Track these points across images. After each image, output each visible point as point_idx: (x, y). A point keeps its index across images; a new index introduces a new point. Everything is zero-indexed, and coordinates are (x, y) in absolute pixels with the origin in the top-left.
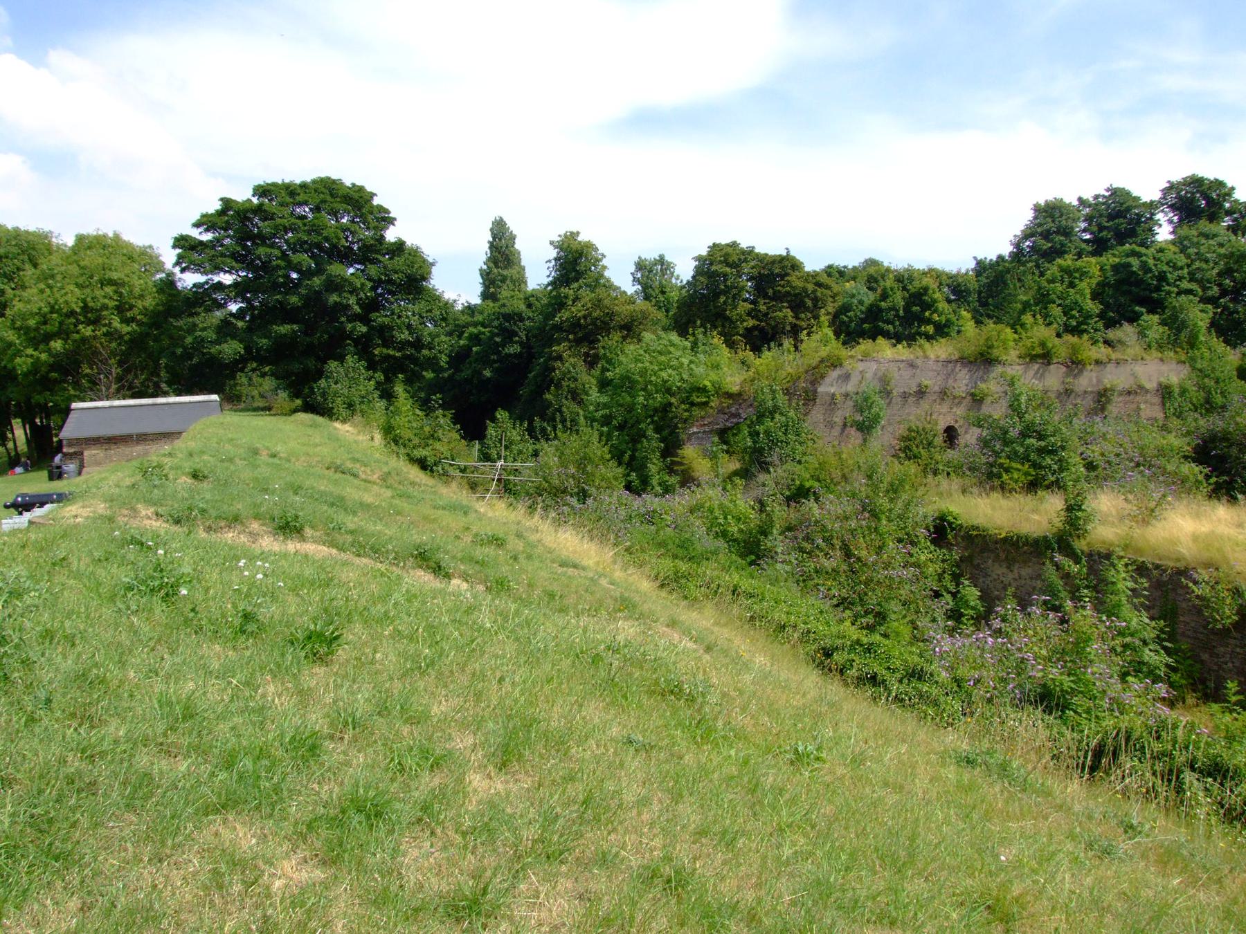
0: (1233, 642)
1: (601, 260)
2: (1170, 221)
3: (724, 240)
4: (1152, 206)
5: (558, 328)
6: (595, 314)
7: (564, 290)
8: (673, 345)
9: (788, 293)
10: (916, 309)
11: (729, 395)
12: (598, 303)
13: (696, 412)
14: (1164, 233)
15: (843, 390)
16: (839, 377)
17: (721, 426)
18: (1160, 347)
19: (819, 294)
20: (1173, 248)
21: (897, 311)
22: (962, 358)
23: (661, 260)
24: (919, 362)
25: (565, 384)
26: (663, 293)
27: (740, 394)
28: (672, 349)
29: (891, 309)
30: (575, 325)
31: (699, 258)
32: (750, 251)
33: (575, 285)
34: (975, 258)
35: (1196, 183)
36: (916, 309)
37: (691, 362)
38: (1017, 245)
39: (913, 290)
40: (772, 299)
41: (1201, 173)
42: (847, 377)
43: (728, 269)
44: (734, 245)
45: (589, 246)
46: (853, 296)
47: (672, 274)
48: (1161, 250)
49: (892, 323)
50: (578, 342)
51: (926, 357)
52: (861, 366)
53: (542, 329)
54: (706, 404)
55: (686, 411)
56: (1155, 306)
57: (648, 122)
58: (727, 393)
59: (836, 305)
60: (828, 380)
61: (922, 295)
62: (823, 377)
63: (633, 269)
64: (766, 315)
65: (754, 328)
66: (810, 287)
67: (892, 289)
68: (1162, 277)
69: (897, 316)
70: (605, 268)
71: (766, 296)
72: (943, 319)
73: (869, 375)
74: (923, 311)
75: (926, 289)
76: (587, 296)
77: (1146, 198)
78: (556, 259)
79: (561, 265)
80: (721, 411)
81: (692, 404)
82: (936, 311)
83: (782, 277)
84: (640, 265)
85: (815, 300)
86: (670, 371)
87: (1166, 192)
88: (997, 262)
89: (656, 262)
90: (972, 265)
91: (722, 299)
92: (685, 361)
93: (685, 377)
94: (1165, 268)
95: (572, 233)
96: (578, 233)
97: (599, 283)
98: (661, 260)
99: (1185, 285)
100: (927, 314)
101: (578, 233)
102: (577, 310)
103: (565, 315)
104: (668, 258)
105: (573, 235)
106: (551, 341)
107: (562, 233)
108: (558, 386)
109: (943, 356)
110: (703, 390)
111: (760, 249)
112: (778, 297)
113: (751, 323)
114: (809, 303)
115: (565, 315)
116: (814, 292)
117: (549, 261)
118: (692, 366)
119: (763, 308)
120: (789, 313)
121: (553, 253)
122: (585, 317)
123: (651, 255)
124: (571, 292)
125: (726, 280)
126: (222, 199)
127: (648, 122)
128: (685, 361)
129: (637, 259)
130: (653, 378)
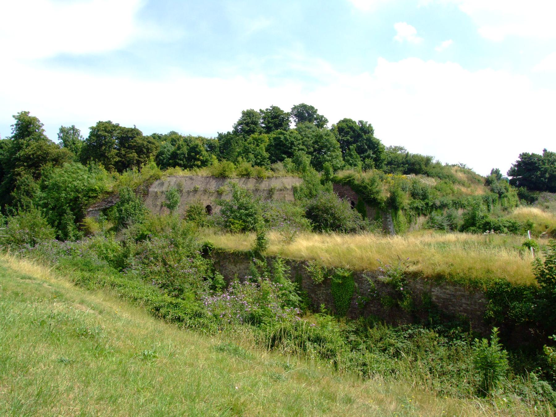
1: (41, 127)
2: (295, 121)
3: (105, 120)
4: (288, 114)
5: (18, 159)
6: (39, 153)
7: (21, 141)
8: (79, 169)
9: (135, 146)
10: (193, 154)
11: (108, 193)
12: (40, 148)
13: (91, 201)
14: (293, 126)
15: (161, 190)
16: (159, 184)
17: (104, 207)
18: (292, 172)
19: (149, 146)
20: (296, 132)
21: (185, 155)
22: (213, 176)
23: (73, 128)
24: (194, 177)
25: (22, 187)
26: (74, 144)
27: (112, 192)
28: (79, 171)
29: (182, 154)
30: (27, 158)
31: (92, 128)
32: (117, 126)
33: (28, 138)
35: (304, 106)
36: (193, 154)
37: (89, 177)
38: (236, 128)
39: (191, 146)
40: (128, 148)
42: (162, 184)
43: (106, 134)
44: (109, 122)
45: (35, 119)
46: (165, 148)
47: (79, 135)
48: (292, 133)
49: (183, 160)
50: (29, 167)
51: (197, 175)
52: (169, 179)
53: (9, 160)
54: (96, 197)
55: (86, 200)
56: (290, 155)
58: (106, 192)
59: (157, 151)
60: (154, 185)
61: (195, 148)
62: (151, 184)
63: (58, 131)
64: (125, 155)
65: (119, 161)
66: (145, 143)
67: (182, 145)
68: (292, 143)
69: (184, 157)
70: (43, 130)
71: (124, 147)
72: (205, 159)
73: (172, 183)
74: (196, 155)
75: (197, 145)
76: (34, 144)
78: (16, 125)
79: (19, 128)
80: (104, 200)
81: (89, 197)
82: (201, 155)
83: (132, 138)
84: (62, 130)
85: (148, 149)
86: (78, 182)
88: (531, 156)
89: (70, 129)
90: (217, 135)
91: (104, 148)
92: (86, 177)
93: (86, 184)
94: (293, 140)
95: (25, 112)
96: (29, 113)
97: (40, 137)
98: (73, 128)
100: (198, 156)
101: (29, 113)
102: (28, 151)
103: (22, 153)
104: (76, 127)
105: (26, 113)
106: (14, 166)
107: (20, 112)
108: (19, 188)
109: (205, 175)
110: (95, 190)
111: (122, 125)
112: (130, 147)
113: (117, 159)
114: (145, 151)
115: (22, 153)
116: (147, 145)
117: (13, 126)
118: (89, 179)
119: (123, 152)
120: (136, 155)
121: (15, 122)
122: (33, 154)
123: (68, 125)
124: (25, 142)
125: (105, 139)
128: (86, 177)
129: (60, 127)
130: (70, 185)
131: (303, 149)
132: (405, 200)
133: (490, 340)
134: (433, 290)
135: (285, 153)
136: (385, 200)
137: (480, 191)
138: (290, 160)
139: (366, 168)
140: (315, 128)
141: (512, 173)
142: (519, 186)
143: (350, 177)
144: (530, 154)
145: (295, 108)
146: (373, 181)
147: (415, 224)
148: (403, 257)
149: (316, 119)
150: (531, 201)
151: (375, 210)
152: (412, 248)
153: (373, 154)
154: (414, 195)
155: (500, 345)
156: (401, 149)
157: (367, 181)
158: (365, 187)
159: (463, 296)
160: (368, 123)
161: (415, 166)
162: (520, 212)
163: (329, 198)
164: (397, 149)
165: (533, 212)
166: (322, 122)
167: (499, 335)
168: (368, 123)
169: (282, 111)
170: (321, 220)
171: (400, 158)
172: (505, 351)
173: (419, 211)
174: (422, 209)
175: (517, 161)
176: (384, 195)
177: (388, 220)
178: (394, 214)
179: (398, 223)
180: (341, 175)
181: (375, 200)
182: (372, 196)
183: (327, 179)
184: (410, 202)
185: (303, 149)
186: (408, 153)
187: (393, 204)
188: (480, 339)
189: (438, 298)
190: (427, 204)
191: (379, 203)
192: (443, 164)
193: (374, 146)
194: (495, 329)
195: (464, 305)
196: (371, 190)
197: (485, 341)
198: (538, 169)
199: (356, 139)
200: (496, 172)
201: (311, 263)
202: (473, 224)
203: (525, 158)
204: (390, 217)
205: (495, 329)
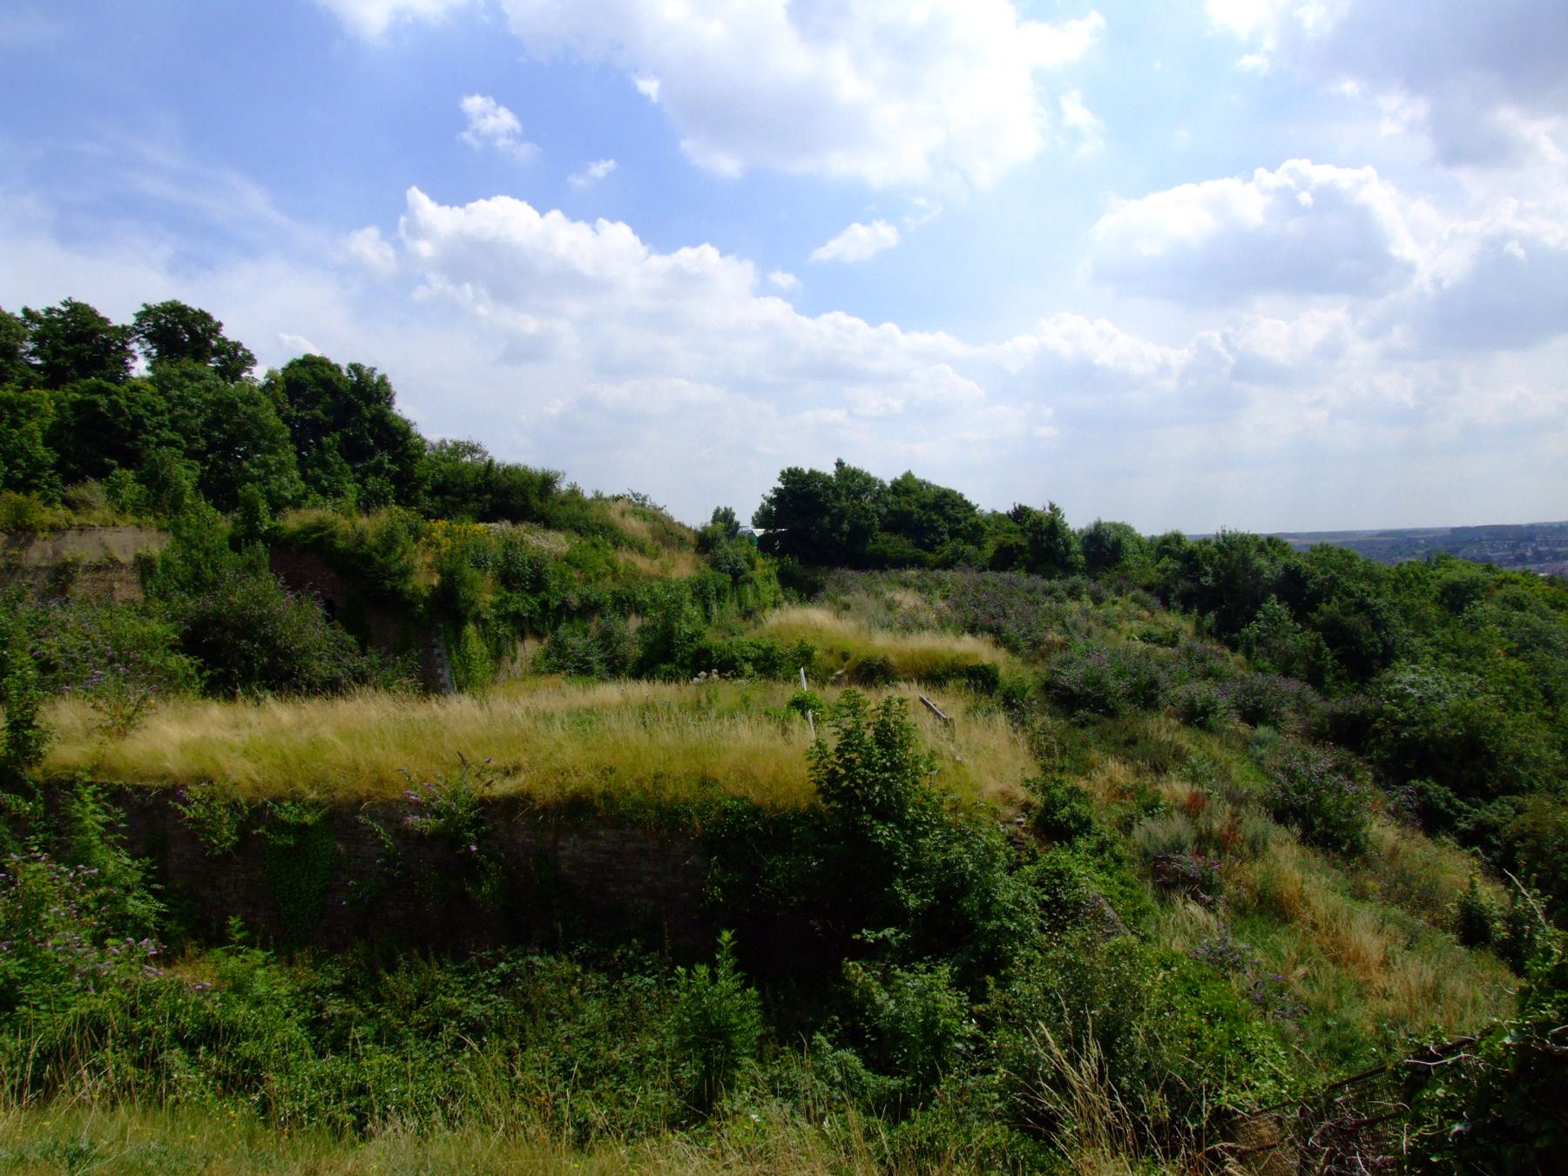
2: (148, 355)
4: (124, 332)
14: (140, 367)
18: (137, 511)
34: (1052, 507)
48: (136, 389)
56: (130, 459)
68: (138, 422)
94: (141, 412)
99: (166, 434)
126: (1052, 507)
132: (485, 594)
133: (713, 964)
134: (561, 843)
136: (426, 594)
143: (323, 529)
144: (806, 471)
145: (148, 313)
149: (216, 352)
150: (808, 592)
153: (391, 462)
154: (508, 578)
156: (473, 450)
157: (372, 540)
158: (367, 559)
160: (379, 373)
161: (517, 496)
162: (783, 620)
164: (459, 449)
165: (813, 621)
166: (235, 360)
167: (735, 951)
168: (379, 373)
170: (230, 659)
171: (469, 476)
173: (524, 626)
175: (776, 491)
177: (436, 651)
180: (292, 521)
181: (396, 594)
184: (496, 599)
186: (491, 461)
187: (449, 606)
191: (410, 605)
196: (383, 568)
198: (823, 510)
200: (725, 518)
201: (196, 791)
203: (795, 482)
204: (442, 644)
205: (726, 936)
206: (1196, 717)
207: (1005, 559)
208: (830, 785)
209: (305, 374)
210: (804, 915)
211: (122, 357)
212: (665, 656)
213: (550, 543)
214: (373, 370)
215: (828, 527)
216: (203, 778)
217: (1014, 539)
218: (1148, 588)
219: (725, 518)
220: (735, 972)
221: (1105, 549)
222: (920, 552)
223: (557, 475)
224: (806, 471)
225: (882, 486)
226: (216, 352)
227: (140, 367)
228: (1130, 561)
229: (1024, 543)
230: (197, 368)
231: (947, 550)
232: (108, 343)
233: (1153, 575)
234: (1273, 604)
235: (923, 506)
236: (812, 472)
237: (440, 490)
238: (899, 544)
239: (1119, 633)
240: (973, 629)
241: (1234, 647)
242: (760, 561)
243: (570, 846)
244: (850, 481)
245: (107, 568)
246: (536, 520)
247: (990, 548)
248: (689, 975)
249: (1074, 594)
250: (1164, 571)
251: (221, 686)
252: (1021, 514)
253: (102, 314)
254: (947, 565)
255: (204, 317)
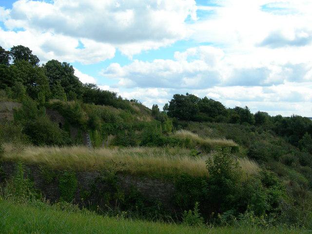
0: (52, 186)
2: (13, 58)
4: (8, 52)
14: (11, 62)
18: (13, 98)
20: (15, 66)
34: (246, 107)
35: (21, 47)
41: (282, 115)
48: (11, 67)
56: (10, 85)
57: (264, 8)
68: (12, 75)
77: (6, 50)
87: (13, 49)
94: (13, 72)
99: (19, 78)
126: (246, 107)
127: (264, 8)
131: (21, 81)
132: (99, 122)
133: (193, 210)
134: (138, 184)
135: (6, 82)
137: (149, 119)
138: (10, 88)
139: (70, 98)
140: (29, 65)
141: (165, 108)
142: (173, 117)
144: (180, 95)
145: (14, 48)
146: (76, 108)
147: (107, 141)
148: (114, 161)
149: (30, 58)
150: (185, 127)
151: (75, 128)
152: (104, 154)
154: (104, 119)
155: (200, 214)
157: (72, 107)
159: (159, 187)
161: (106, 98)
163: (45, 119)
164: (91, 85)
165: (184, 133)
166: (35, 60)
167: (199, 207)
169: (4, 50)
170: (36, 136)
172: (202, 218)
173: (109, 132)
174: (111, 131)
176: (84, 117)
177: (87, 137)
178: (91, 134)
179: (93, 138)
180: (51, 102)
181: (77, 122)
182: (76, 119)
183: (41, 105)
184: (103, 125)
185: (21, 81)
186: (99, 89)
187: (91, 125)
188: (188, 211)
189: (142, 189)
190: (115, 127)
192: (124, 99)
193: (75, 81)
194: (197, 203)
195: (160, 193)
197: (190, 211)
199: (60, 73)
200: (155, 107)
201: (41, 167)
202: (151, 141)
205: (197, 203)
206: (288, 163)
207: (234, 120)
208: (211, 169)
209: (52, 65)
210: (213, 197)
211: (6, 60)
212: (149, 141)
213: (117, 112)
214: (69, 64)
215: (188, 110)
216: (43, 164)
217: (236, 115)
218: (273, 129)
219: (155, 107)
220: (198, 213)
221: (261, 118)
222: (211, 118)
223: (116, 93)
224: (180, 95)
225: (200, 99)
226: (30, 58)
227: (11, 62)
228: (267, 122)
229: (239, 116)
230: (26, 62)
231: (218, 117)
232: (4, 55)
233: (274, 126)
234: (307, 134)
235: (211, 106)
236: (182, 95)
237: (85, 96)
238: (204, 115)
239: (267, 141)
240: (228, 138)
241: (296, 146)
242: (168, 119)
243: (140, 185)
244: (192, 98)
245: (6, 112)
246: (110, 105)
247: (229, 118)
248: (187, 213)
249: (253, 130)
250: (277, 125)
251: (36, 143)
252: (237, 109)
253: (26, 46)
254: (218, 121)
255: (27, 49)
